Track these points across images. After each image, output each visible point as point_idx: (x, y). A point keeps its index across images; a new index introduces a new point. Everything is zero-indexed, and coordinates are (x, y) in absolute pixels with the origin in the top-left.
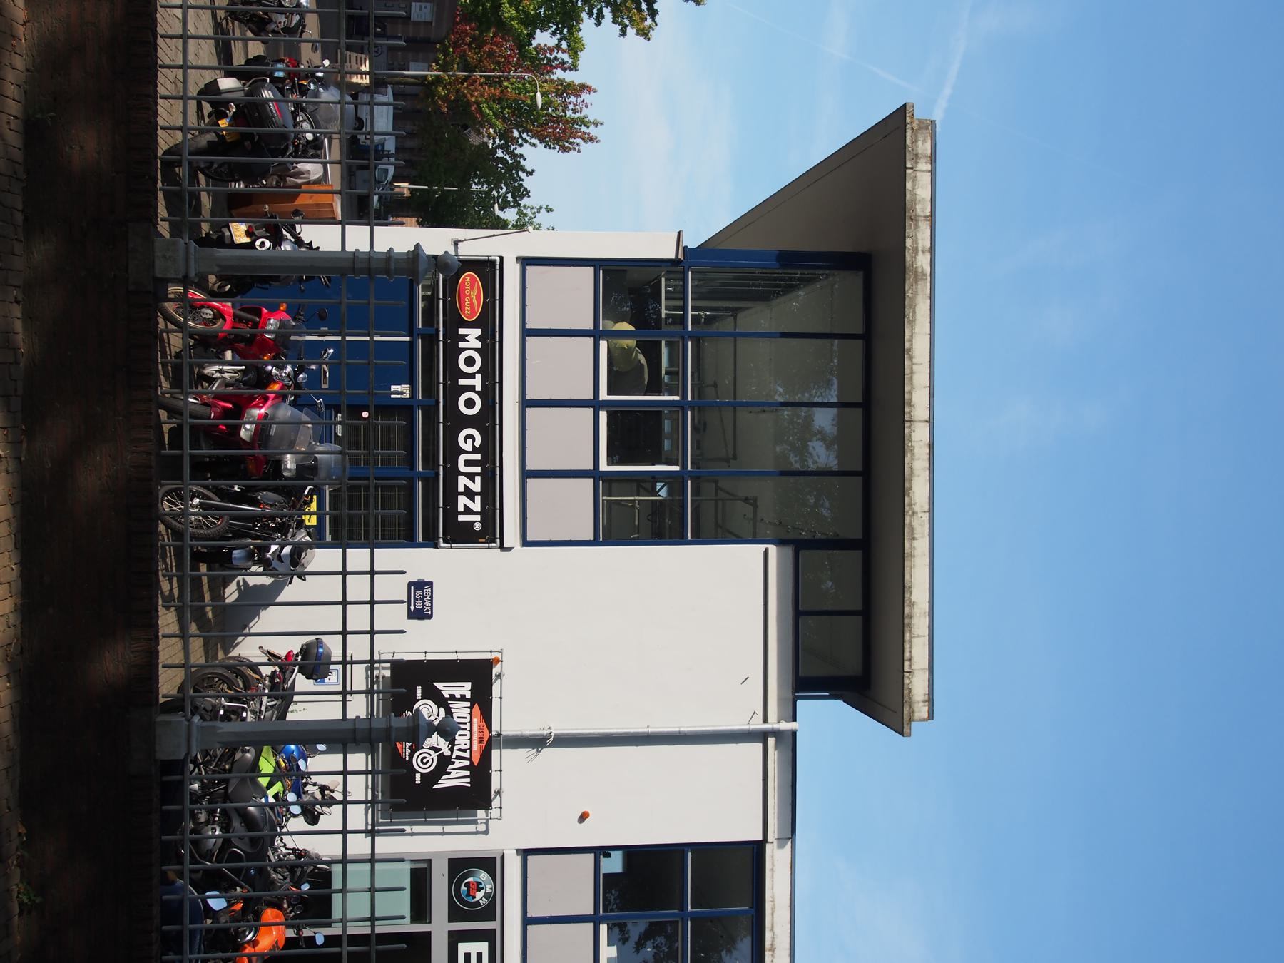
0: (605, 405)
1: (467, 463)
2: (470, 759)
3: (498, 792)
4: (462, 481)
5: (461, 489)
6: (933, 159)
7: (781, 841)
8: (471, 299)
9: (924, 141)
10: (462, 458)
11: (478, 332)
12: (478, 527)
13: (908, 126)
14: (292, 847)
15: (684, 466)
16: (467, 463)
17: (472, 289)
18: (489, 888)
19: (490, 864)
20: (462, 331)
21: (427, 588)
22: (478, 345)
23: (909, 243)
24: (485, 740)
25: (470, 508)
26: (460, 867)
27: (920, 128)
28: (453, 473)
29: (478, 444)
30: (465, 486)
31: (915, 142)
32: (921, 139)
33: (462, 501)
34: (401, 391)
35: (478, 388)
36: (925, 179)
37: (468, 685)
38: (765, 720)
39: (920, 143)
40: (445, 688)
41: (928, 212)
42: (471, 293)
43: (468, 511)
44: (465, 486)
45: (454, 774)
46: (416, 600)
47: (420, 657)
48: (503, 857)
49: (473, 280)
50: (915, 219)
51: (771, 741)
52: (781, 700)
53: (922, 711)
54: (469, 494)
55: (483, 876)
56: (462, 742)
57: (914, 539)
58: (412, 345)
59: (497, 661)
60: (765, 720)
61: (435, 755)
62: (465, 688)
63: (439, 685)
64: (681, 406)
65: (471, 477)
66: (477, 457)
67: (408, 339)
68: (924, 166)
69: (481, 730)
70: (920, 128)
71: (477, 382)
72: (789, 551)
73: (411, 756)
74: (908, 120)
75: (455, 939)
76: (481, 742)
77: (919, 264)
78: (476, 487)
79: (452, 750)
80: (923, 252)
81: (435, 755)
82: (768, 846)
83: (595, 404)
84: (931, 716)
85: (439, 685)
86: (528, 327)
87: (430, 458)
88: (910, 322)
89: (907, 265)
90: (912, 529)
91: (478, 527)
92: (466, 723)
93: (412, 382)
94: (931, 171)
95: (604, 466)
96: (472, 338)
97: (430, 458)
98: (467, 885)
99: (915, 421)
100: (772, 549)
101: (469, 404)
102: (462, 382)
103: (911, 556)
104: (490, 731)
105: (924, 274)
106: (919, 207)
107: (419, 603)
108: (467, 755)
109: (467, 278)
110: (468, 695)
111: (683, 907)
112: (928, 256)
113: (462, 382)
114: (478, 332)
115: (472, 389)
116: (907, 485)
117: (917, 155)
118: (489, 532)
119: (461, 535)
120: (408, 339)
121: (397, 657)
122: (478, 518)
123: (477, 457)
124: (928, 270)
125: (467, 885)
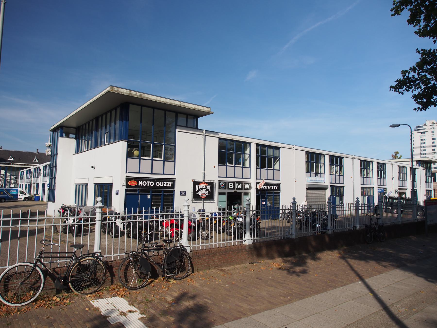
0: (152, 158)
1: (162, 185)
2: (207, 185)
3: (210, 181)
4: (165, 186)
5: (166, 186)
6: (119, 88)
7: (218, 135)
8: (134, 183)
10: (161, 185)
11: (139, 182)
12: (172, 183)
13: (113, 92)
15: (151, 143)
16: (162, 185)
17: (131, 183)
18: (222, 183)
19: (220, 182)
20: (139, 185)
21: (181, 192)
22: (142, 182)
23: (125, 94)
24: (204, 183)
25: (169, 184)
26: (220, 188)
27: (112, 89)
28: (163, 187)
29: (159, 182)
30: (166, 185)
31: (114, 91)
32: (114, 89)
33: (168, 186)
34: (149, 197)
35: (149, 182)
36: (122, 90)
37: (197, 185)
38: (203, 135)
39: (115, 90)
40: (197, 189)
41: (129, 91)
42: (132, 183)
43: (169, 185)
44: (166, 185)
45: (209, 188)
46: (183, 194)
47: (192, 193)
48: (219, 181)
49: (130, 182)
50: (130, 94)
51: (206, 135)
52: (199, 132)
53: (209, 109)
54: (167, 184)
55: (221, 184)
56: (204, 187)
57: (184, 106)
58: (141, 194)
59: (193, 181)
60: (203, 135)
61: (206, 191)
62: (197, 186)
63: (196, 191)
64: (153, 143)
65: (164, 184)
66: (161, 182)
67: (139, 195)
68: (120, 90)
69: (203, 184)
70: (112, 89)
71: (148, 182)
72: (177, 127)
73: (206, 195)
74: (112, 91)
75: (229, 189)
76: (205, 184)
77: (139, 95)
78: (166, 183)
79: (205, 188)
80: (136, 93)
81: (206, 191)
82: (220, 137)
83: (152, 160)
84: (210, 108)
85: (196, 191)
86: (138, 172)
87: (160, 191)
88: (150, 99)
89: (129, 95)
90: (184, 106)
91: (172, 183)
93: (147, 194)
94: (121, 88)
95: (163, 159)
96: (140, 183)
97: (160, 191)
98: (222, 186)
100: (177, 130)
101: (152, 184)
102: (148, 185)
103: (160, 101)
104: (203, 182)
105: (140, 94)
106: (128, 93)
107: (184, 194)
108: (206, 186)
109: (129, 184)
110: (198, 185)
111: (226, 152)
112: (137, 93)
113: (148, 185)
114: (139, 182)
115: (149, 183)
116: (177, 105)
117: (118, 91)
118: (173, 181)
119: (173, 186)
120: (139, 195)
121: (192, 197)
122: (171, 183)
123: (161, 182)
124: (140, 93)
125: (222, 186)
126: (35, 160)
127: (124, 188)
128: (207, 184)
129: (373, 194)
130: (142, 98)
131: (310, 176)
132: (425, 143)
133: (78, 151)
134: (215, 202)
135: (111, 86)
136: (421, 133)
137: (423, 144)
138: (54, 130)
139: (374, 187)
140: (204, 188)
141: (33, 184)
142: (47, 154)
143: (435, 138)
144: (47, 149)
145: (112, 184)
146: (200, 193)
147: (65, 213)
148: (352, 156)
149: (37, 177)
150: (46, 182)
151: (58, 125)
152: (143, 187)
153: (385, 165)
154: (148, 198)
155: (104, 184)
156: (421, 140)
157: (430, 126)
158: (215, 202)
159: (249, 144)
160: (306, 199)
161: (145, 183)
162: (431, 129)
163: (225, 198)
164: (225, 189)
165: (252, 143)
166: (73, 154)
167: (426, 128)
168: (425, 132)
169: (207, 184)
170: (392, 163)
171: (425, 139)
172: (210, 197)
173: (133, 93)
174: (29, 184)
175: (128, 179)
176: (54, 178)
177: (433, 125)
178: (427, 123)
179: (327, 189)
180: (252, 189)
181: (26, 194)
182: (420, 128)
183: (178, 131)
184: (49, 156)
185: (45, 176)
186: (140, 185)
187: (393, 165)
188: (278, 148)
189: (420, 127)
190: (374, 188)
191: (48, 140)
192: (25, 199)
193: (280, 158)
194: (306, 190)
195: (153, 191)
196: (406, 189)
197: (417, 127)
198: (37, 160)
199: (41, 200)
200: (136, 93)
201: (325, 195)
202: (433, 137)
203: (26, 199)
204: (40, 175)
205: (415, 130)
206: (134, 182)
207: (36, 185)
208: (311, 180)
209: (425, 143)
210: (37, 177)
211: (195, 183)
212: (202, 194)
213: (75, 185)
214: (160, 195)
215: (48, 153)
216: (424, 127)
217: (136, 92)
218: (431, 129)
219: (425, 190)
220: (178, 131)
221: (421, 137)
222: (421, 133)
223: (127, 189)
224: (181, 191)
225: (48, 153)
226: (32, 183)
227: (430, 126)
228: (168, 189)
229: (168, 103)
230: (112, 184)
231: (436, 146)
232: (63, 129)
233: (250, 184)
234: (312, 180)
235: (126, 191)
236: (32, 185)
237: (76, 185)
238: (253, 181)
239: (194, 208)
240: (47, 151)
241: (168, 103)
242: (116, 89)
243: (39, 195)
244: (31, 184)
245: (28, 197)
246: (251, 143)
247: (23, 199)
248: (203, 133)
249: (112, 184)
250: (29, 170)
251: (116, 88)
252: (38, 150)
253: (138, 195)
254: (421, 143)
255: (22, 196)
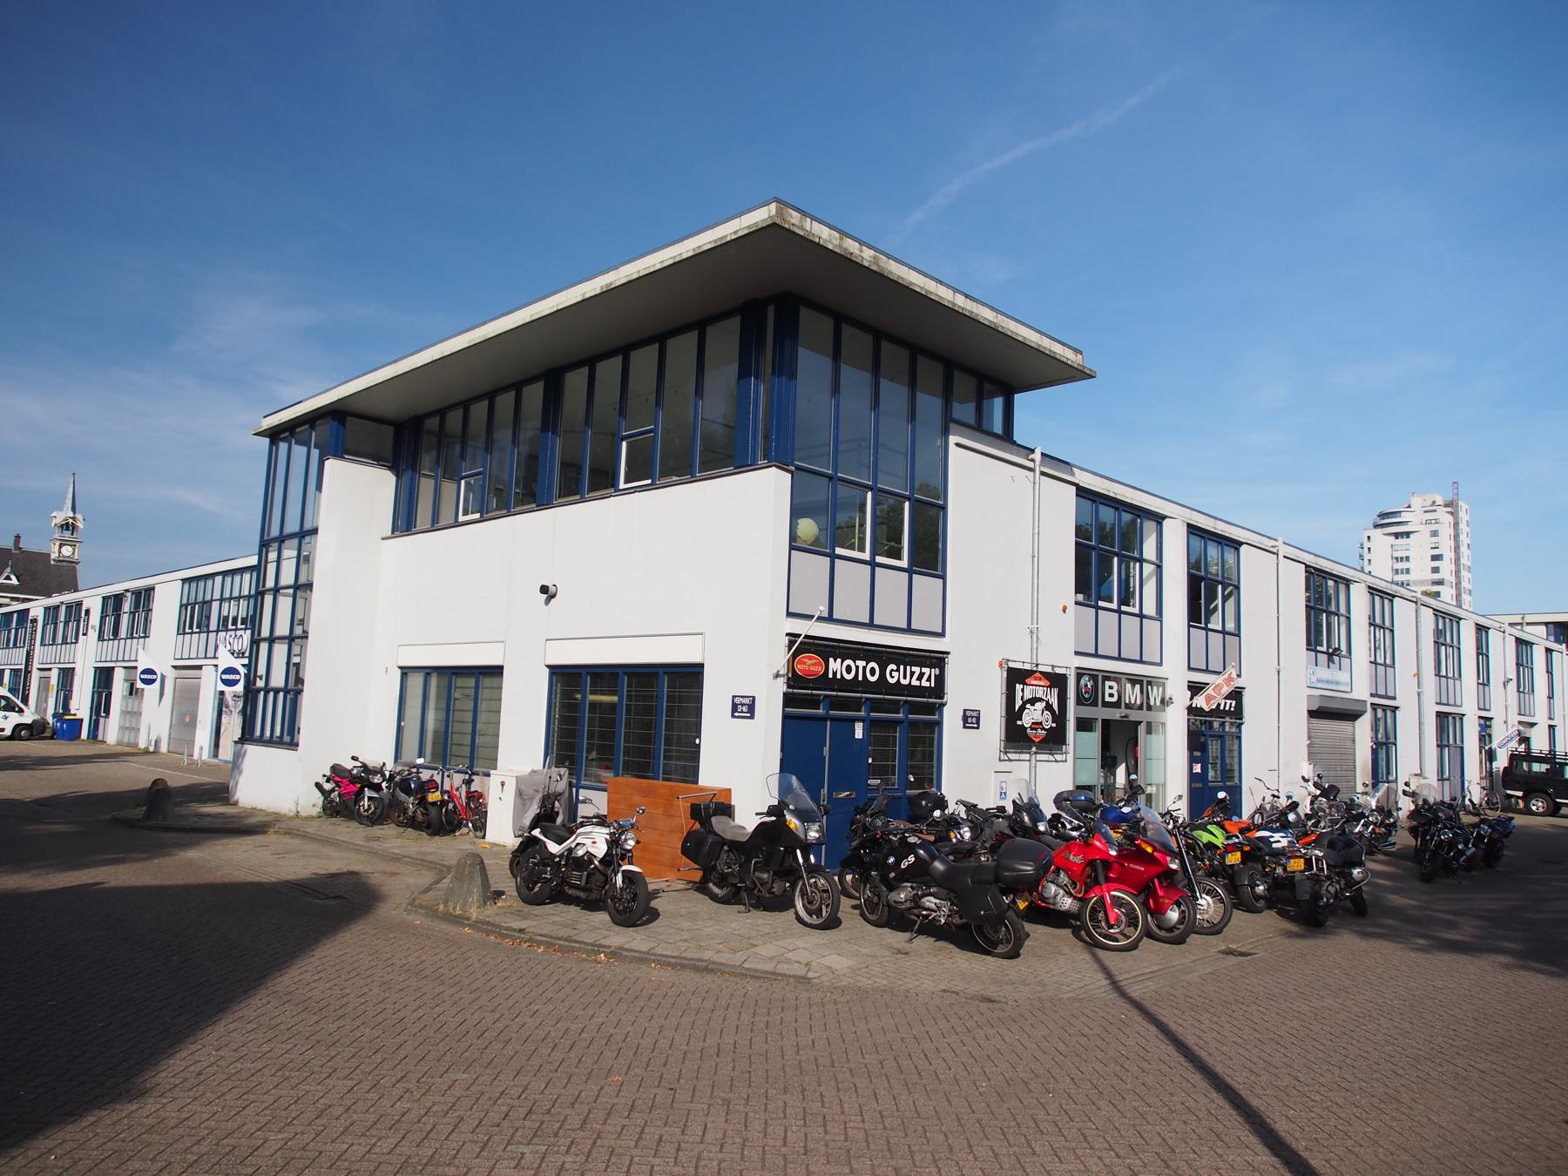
0: (873, 557)
1: (905, 678)
4: (915, 683)
7: (1072, 474)
8: (812, 664)
9: (791, 215)
10: (904, 682)
14: (995, 807)
16: (905, 678)
17: (804, 663)
20: (831, 676)
29: (894, 667)
34: (859, 732)
35: (864, 663)
37: (1017, 685)
45: (1053, 700)
50: (840, 246)
56: (1040, 693)
58: (833, 719)
61: (1046, 712)
62: (1019, 687)
65: (912, 673)
67: (828, 722)
68: (808, 223)
71: (861, 664)
73: (1045, 730)
75: (1106, 705)
76: (1040, 679)
82: (1081, 484)
92: (1226, 703)
93: (854, 720)
99: (721, 424)
100: (953, 439)
101: (867, 670)
102: (860, 678)
109: (798, 668)
113: (860, 678)
114: (831, 660)
115: (864, 668)
116: (993, 326)
118: (937, 660)
120: (828, 722)
125: (1085, 693)
126: (8, 578)
127: (781, 687)
128: (1048, 683)
129: (1463, 743)
130: (883, 276)
131: (1340, 669)
132: (1408, 571)
133: (404, 522)
134: (1066, 761)
135: (778, 201)
136: (1397, 535)
137: (1402, 573)
138: (275, 435)
139: (1464, 715)
140: (1040, 700)
141: (39, 669)
142: (54, 556)
143: (1442, 555)
144: (56, 536)
145: (500, 671)
146: (1027, 720)
147: (366, 799)
148: (1414, 594)
149: (65, 642)
150: (74, 663)
151: (327, 405)
152: (842, 684)
153: (1487, 632)
154: (856, 737)
155: (579, 671)
156: (1397, 558)
157: (1425, 512)
158: (1066, 761)
159: (1153, 524)
160: (1309, 753)
161: (849, 669)
162: (1428, 522)
163: (1093, 739)
164: (1095, 704)
165: (1167, 520)
166: (384, 535)
167: (1413, 519)
168: (1407, 534)
169: (1048, 683)
170: (1502, 625)
171: (1407, 559)
172: (1054, 740)
173: (852, 246)
174: (15, 672)
175: (802, 646)
176: (264, 639)
177: (1435, 511)
178: (1417, 502)
179: (1361, 716)
180: (1170, 709)
181: (21, 711)
182: (1392, 517)
183: (958, 445)
184: (64, 564)
185: (52, 645)
186: (835, 674)
187: (1507, 634)
188: (1236, 545)
189: (1390, 516)
190: (1464, 718)
191: (64, 503)
192: (21, 727)
193: (1237, 588)
194: (1308, 720)
195: (877, 706)
196: (1532, 725)
197: (1383, 515)
198: (13, 577)
199: (84, 735)
200: (861, 251)
201: (1354, 741)
202: (1435, 552)
203: (23, 733)
204: (84, 634)
205: (1376, 526)
206: (814, 661)
207: (54, 675)
208: (1318, 681)
209: (1408, 571)
210: (65, 642)
211: (1016, 677)
212: (1033, 723)
213: (399, 670)
214: (895, 723)
215: (60, 552)
216: (1404, 517)
217: (862, 243)
218: (1428, 522)
219: (1547, 727)
220: (958, 445)
221: (1395, 548)
222: (1397, 535)
223: (791, 690)
224: (965, 711)
225: (60, 552)
226: (36, 665)
227: (1425, 512)
228: (882, 696)
229: (966, 310)
230: (701, 666)
231: (1445, 583)
232: (344, 426)
233: (1164, 685)
234: (1323, 681)
235: (788, 700)
236: (35, 676)
237: (405, 671)
238: (1174, 675)
239: (1004, 785)
240: (58, 543)
241: (964, 312)
242: (794, 217)
243: (75, 715)
244: (30, 672)
245: (30, 722)
246: (1164, 517)
247: (8, 732)
248: (1033, 460)
249: (701, 666)
250: (15, 615)
251: (795, 214)
252: (18, 538)
253: (824, 719)
254: (1397, 571)
255: (6, 718)
